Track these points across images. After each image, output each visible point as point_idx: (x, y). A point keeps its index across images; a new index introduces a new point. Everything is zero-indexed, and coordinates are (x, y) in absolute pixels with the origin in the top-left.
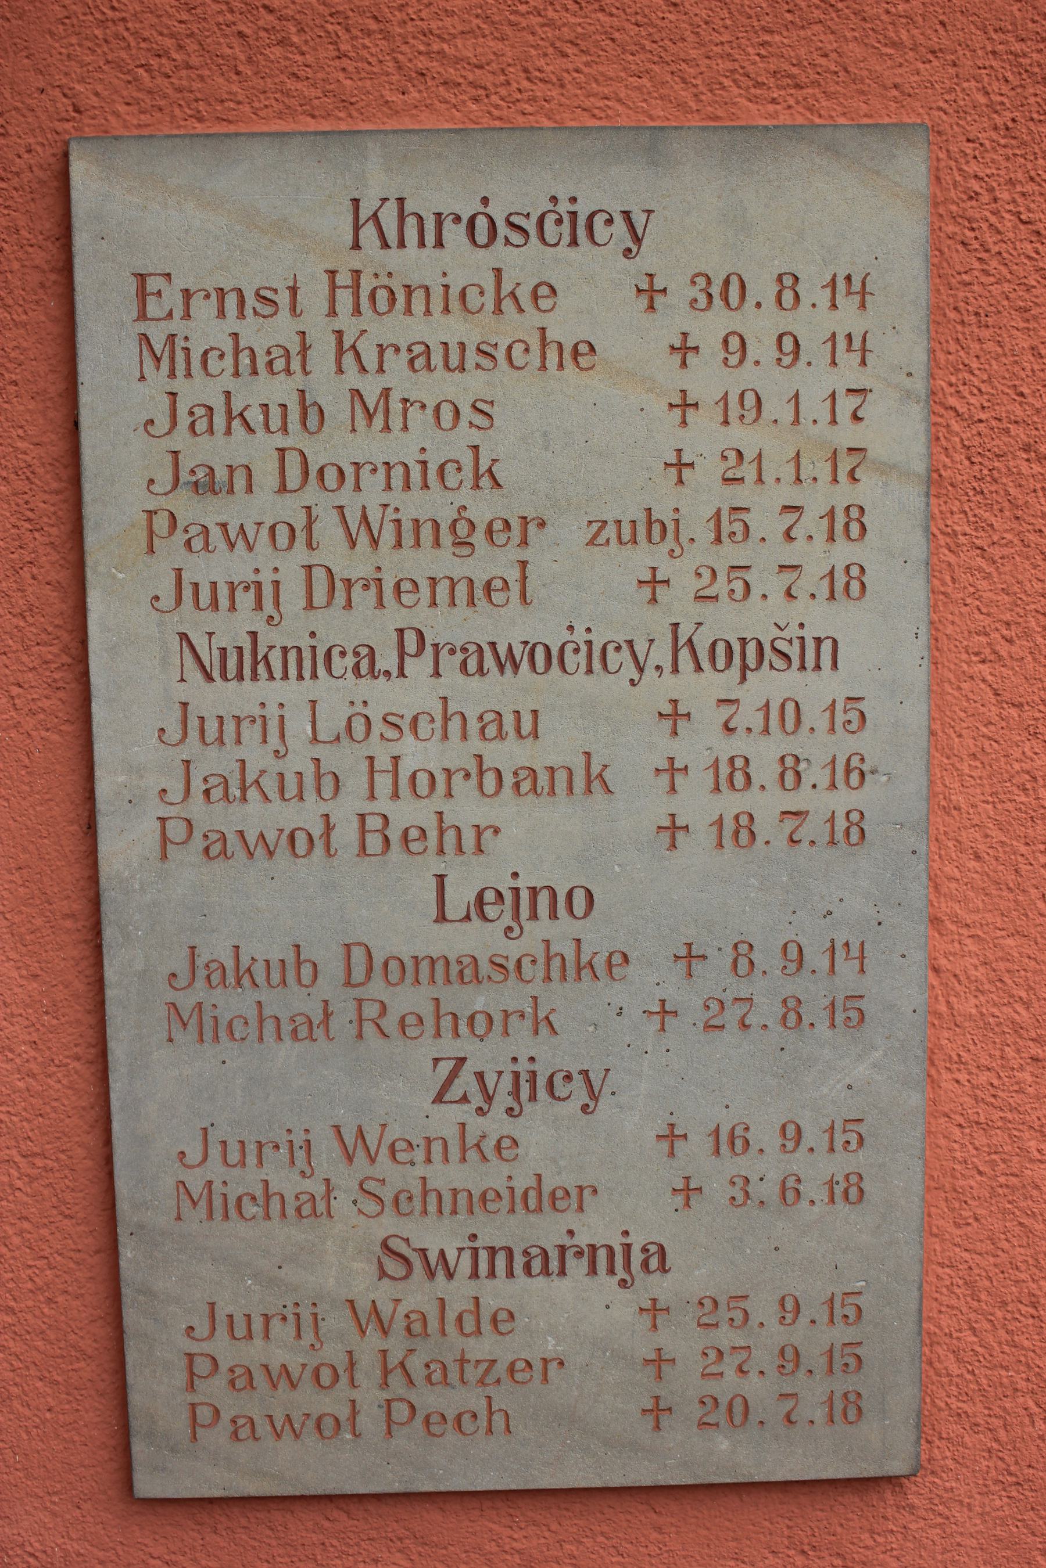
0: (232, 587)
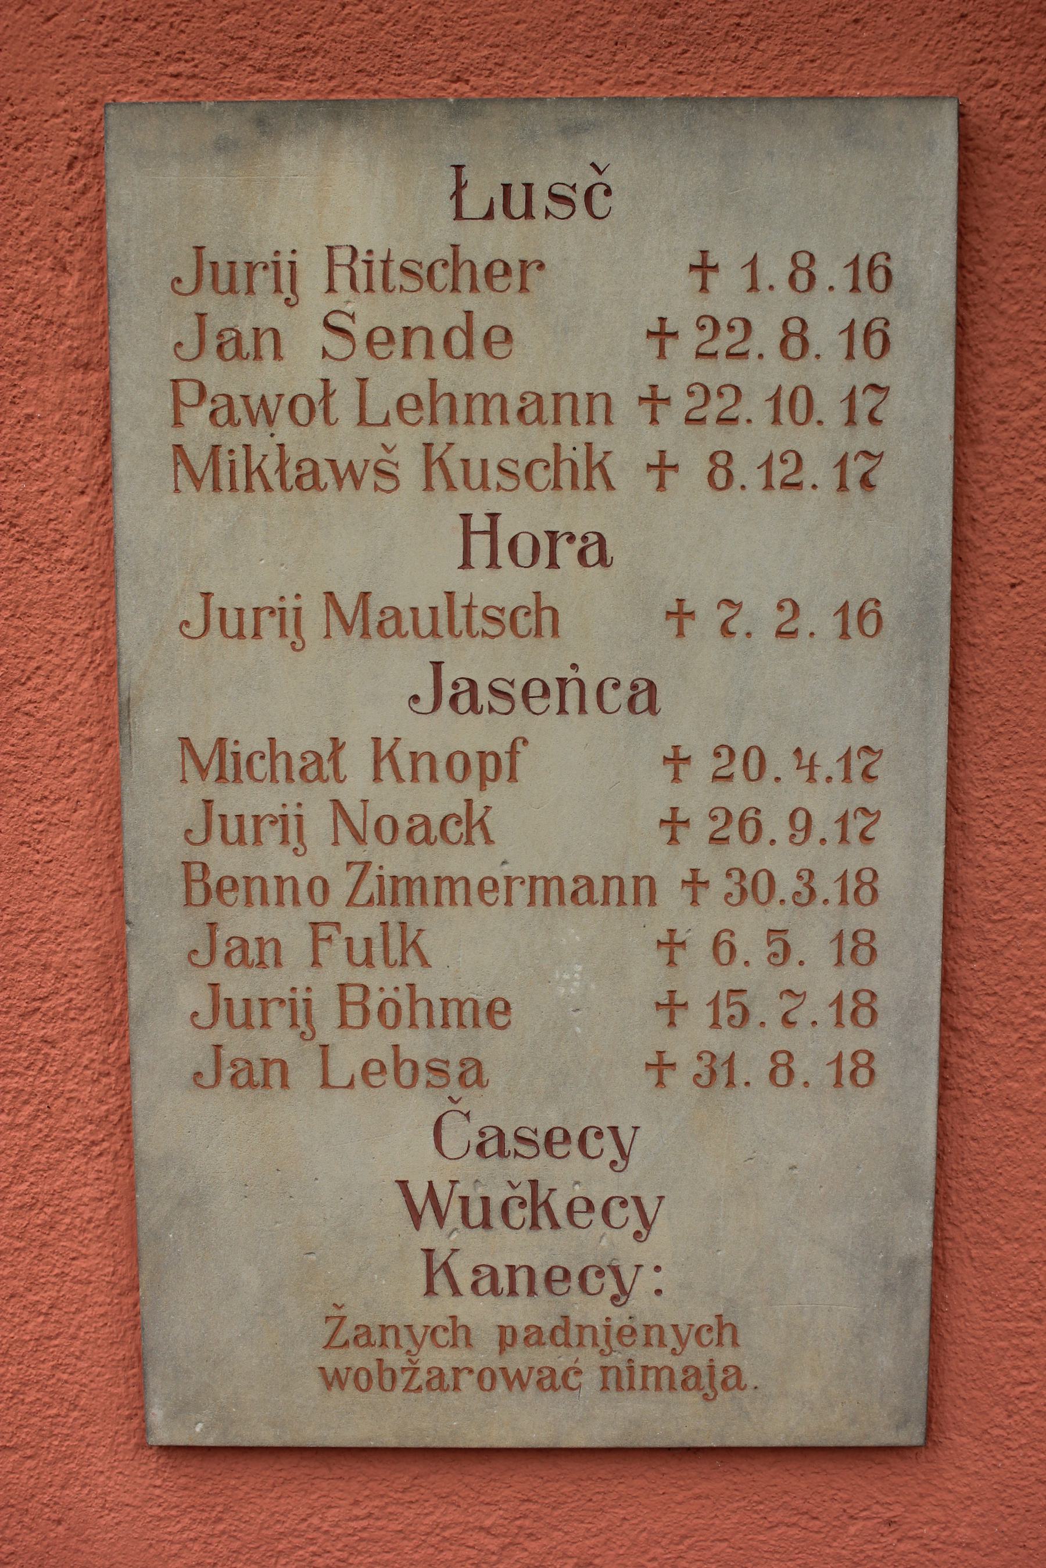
0: (251, 267)
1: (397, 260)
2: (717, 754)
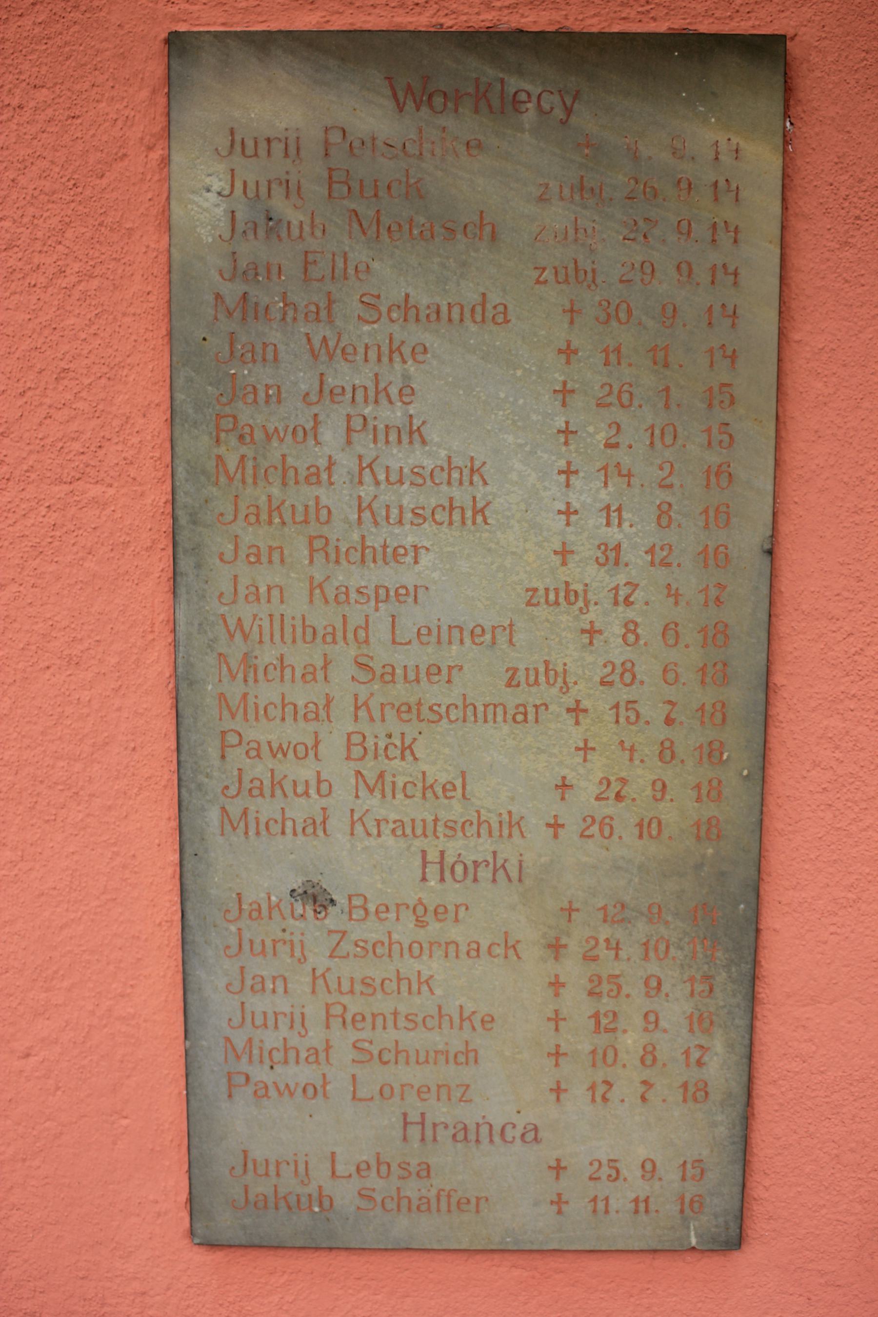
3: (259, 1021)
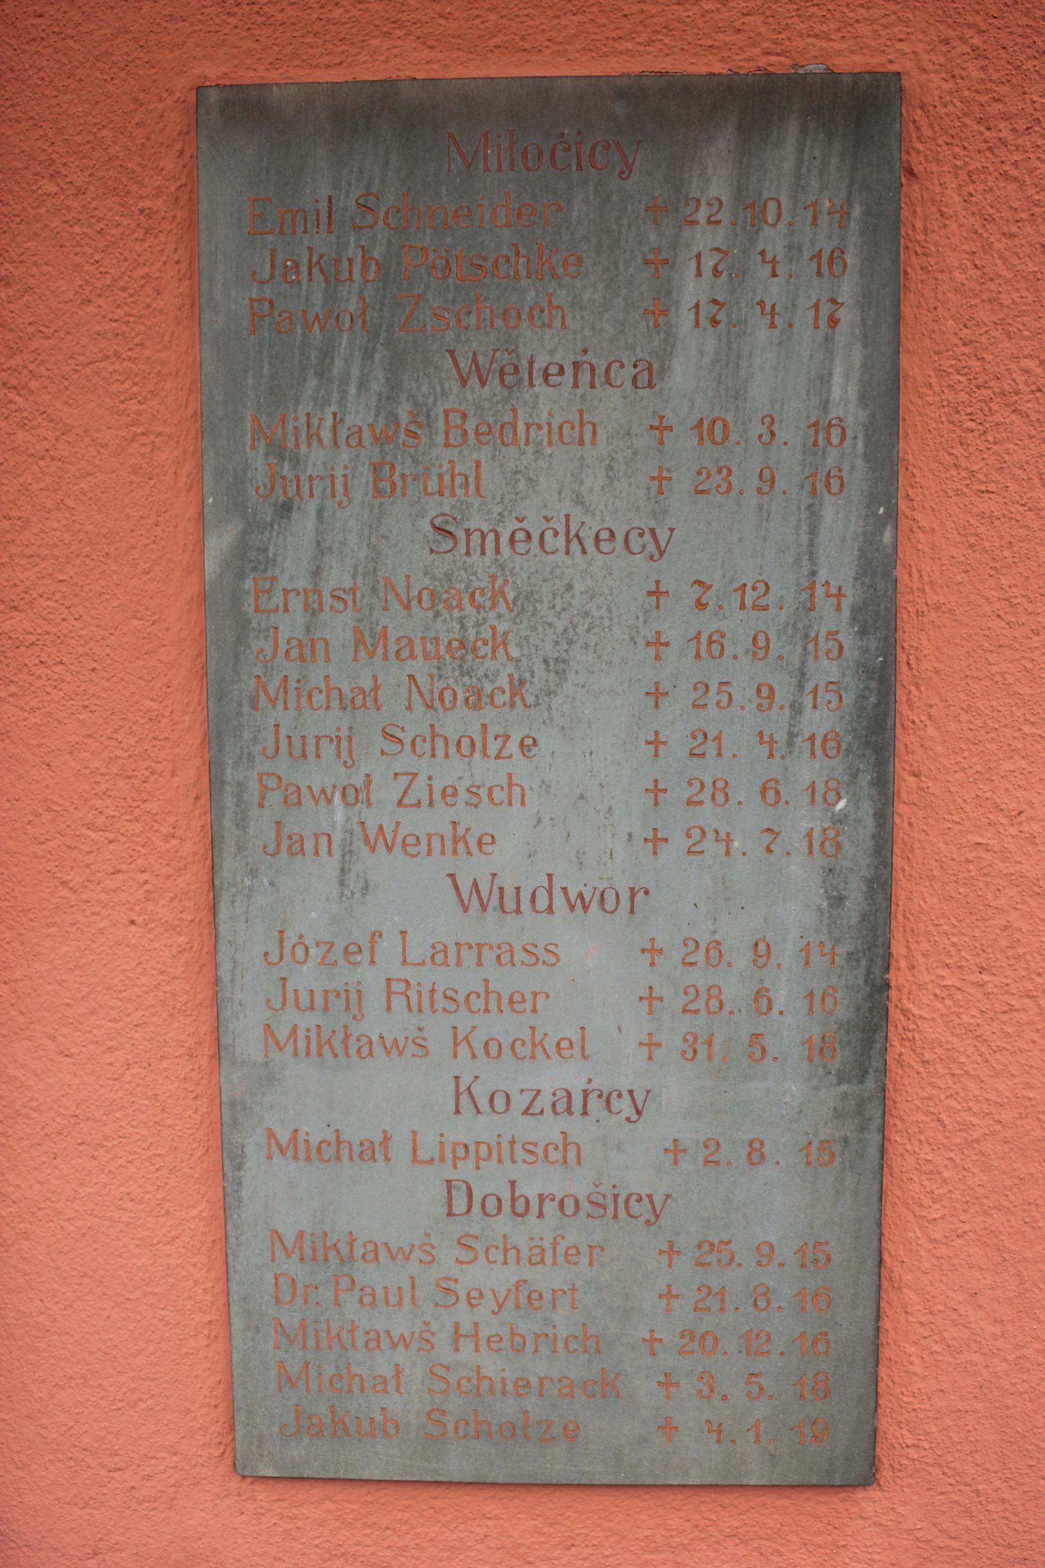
1: (440, 990)
2: (686, 993)
3: (304, 1000)
